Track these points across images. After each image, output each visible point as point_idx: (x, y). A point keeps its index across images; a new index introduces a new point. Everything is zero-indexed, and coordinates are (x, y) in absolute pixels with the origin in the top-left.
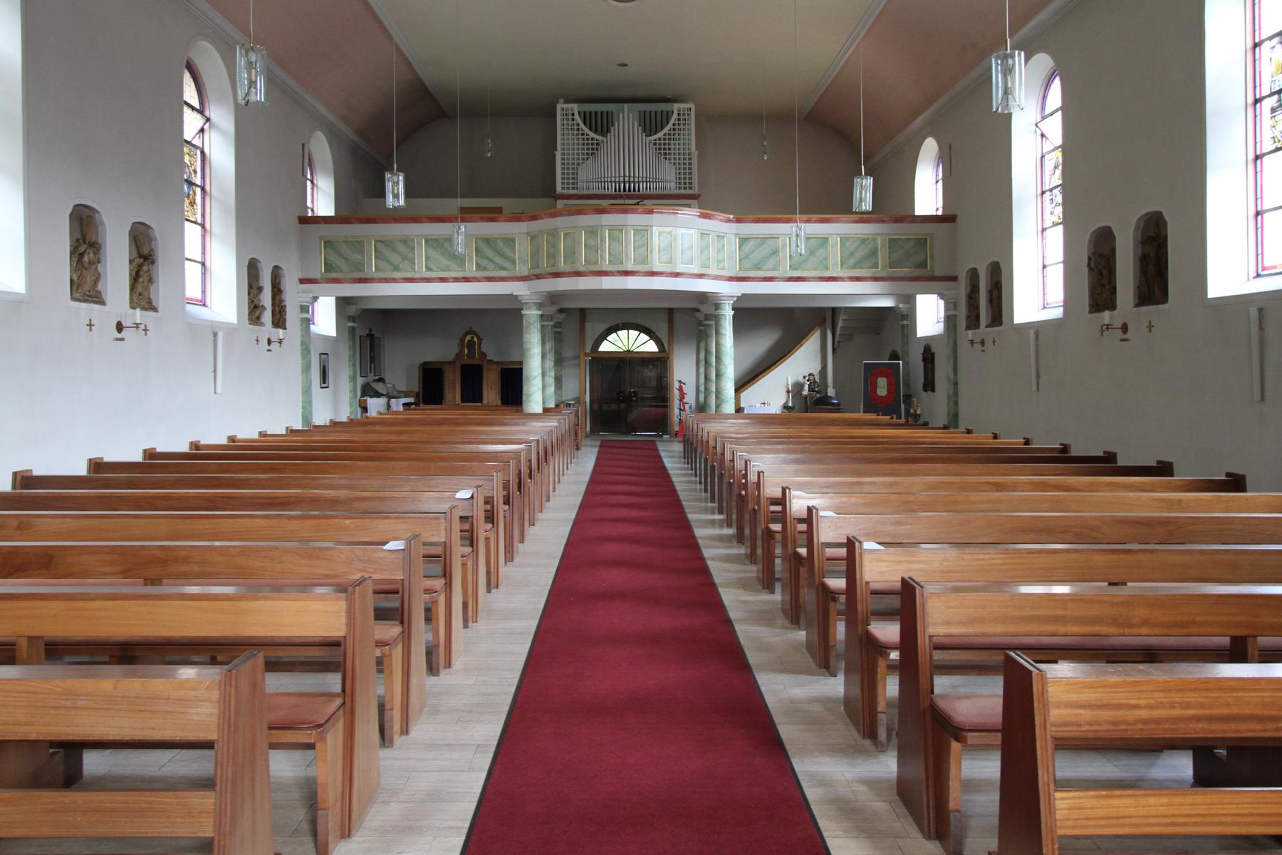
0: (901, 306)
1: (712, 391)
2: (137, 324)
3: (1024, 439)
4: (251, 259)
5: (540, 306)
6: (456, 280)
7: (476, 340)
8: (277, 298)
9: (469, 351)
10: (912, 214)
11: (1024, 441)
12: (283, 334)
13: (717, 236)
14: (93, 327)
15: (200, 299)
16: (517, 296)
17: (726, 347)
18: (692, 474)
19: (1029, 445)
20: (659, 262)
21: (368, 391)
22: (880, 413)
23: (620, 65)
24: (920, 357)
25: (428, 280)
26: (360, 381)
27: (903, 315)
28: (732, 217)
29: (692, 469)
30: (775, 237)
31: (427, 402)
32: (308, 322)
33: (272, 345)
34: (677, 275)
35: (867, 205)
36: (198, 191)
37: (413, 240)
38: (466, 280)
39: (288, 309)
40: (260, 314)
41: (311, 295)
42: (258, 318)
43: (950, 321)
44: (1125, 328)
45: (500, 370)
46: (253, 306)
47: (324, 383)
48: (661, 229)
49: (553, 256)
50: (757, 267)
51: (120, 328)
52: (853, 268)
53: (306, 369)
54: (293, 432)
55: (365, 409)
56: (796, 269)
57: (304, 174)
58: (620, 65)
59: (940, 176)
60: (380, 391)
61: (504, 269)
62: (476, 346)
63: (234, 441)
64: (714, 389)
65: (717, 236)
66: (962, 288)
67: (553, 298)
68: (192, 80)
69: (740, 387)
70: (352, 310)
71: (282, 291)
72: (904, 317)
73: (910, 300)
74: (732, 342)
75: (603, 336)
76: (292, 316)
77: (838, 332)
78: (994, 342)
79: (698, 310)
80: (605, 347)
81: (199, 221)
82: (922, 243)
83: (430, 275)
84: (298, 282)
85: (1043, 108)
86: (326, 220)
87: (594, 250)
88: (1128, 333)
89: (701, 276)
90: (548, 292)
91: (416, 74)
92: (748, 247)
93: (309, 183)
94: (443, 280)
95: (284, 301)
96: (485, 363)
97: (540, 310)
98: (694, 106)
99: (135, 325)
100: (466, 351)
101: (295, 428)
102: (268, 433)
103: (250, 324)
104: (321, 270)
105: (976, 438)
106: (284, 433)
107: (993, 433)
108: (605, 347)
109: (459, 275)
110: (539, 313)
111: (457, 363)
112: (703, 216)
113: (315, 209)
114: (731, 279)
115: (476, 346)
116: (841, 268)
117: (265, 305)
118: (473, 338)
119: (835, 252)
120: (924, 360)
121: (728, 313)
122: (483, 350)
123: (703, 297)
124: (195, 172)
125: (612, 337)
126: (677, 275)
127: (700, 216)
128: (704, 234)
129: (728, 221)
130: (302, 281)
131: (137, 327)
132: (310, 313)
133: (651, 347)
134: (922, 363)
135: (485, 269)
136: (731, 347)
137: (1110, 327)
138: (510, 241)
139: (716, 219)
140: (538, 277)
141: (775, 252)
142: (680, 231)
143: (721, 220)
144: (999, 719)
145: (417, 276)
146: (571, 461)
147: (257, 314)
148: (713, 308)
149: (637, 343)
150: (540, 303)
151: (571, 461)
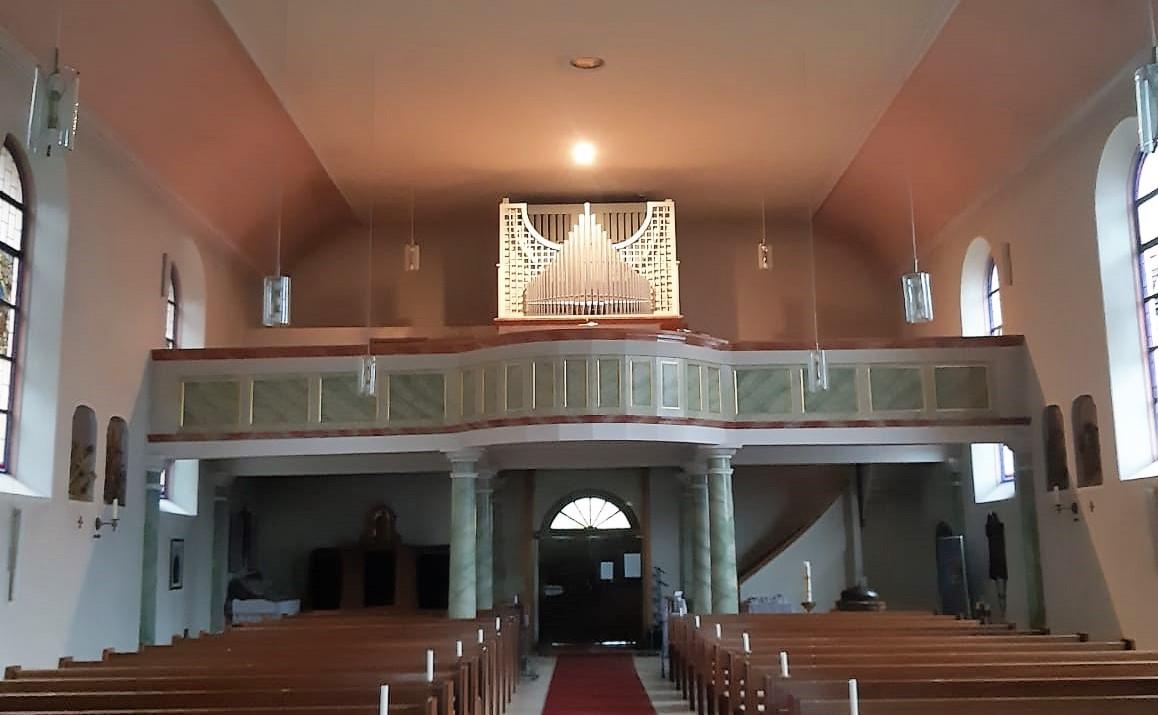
0: (951, 460)
1: (705, 583)
3: (1078, 634)
4: (78, 407)
5: (476, 467)
6: (363, 433)
7: (388, 516)
8: (631, 651)
10: (957, 335)
11: (1123, 643)
12: (119, 511)
13: (709, 368)
16: (443, 453)
17: (724, 519)
18: (686, 706)
19: (1130, 649)
20: (634, 403)
21: (237, 591)
22: (962, 615)
24: (983, 530)
25: (324, 434)
26: (226, 578)
27: (955, 474)
28: (727, 342)
29: (685, 698)
30: (783, 369)
31: (317, 606)
32: (154, 496)
33: (102, 527)
34: (657, 420)
35: (548, 593)
36: (12, 313)
37: (306, 380)
38: (377, 433)
39: (129, 477)
40: (87, 484)
41: (163, 457)
42: (84, 490)
43: (1022, 479)
46: (77, 473)
47: (176, 581)
48: (637, 359)
49: (492, 397)
50: (762, 409)
52: (890, 408)
53: (149, 563)
54: (111, 656)
55: (229, 615)
56: (814, 410)
57: (163, 293)
59: (995, 285)
60: (255, 592)
61: (425, 416)
63: (67, 666)
64: (709, 581)
65: (709, 368)
66: (1037, 433)
67: (492, 453)
68: (14, 165)
69: (745, 570)
70: (221, 479)
71: (121, 453)
72: (956, 476)
73: (963, 454)
74: (732, 512)
75: (557, 509)
76: (134, 486)
77: (867, 496)
78: (1092, 507)
79: (680, 470)
80: (560, 523)
81: (9, 355)
82: (977, 373)
83: (327, 426)
84: (147, 439)
85: (1135, 191)
86: (192, 354)
87: (546, 388)
89: (689, 421)
90: (487, 447)
91: (319, 164)
92: (748, 381)
93: (171, 308)
94: (344, 433)
95: (123, 466)
98: (673, 203)
101: (117, 651)
102: (75, 660)
103: (70, 498)
104: (179, 423)
105: (1054, 640)
106: (100, 659)
107: (1123, 640)
108: (560, 523)
109: (363, 426)
110: (475, 475)
112: (689, 341)
113: (178, 342)
114: (727, 425)
116: (874, 409)
119: (865, 392)
120: (989, 534)
121: (726, 472)
123: (689, 449)
124: (9, 287)
125: (569, 509)
126: (657, 420)
127: (686, 342)
128: (692, 365)
129: (722, 347)
130: (152, 438)
132: (162, 482)
133: (621, 522)
134: (987, 539)
135: (402, 417)
136: (730, 519)
138: (436, 380)
139: (707, 345)
140: (473, 426)
141: (786, 389)
142: (661, 362)
143: (714, 348)
144: (179, 348)
145: (310, 428)
146: (514, 688)
147: (82, 484)
148: (705, 467)
149: (601, 519)
150: (475, 463)
151: (514, 688)
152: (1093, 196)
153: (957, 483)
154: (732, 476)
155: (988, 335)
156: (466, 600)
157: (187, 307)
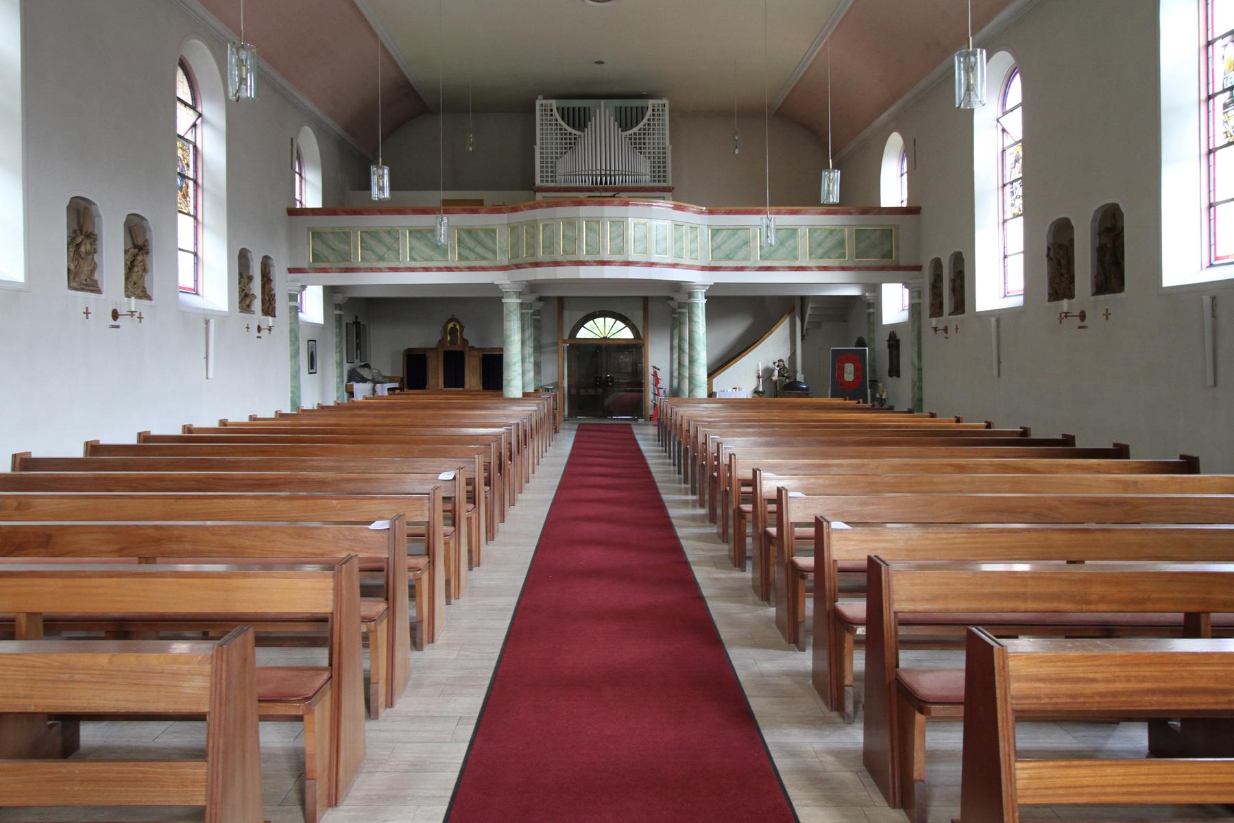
0: (867, 294)
1: (685, 377)
2: (132, 312)
3: (986, 422)
4: (242, 249)
5: (520, 294)
6: (439, 269)
7: (458, 327)
9: (451, 338)
10: (877, 206)
11: (986, 424)
12: (273, 321)
13: (691, 227)
14: (89, 315)
15: (193, 288)
16: (497, 285)
17: (699, 334)
18: (666, 456)
19: (990, 428)
20: (634, 252)
21: (354, 376)
22: (847, 398)
23: (597, 63)
24: (886, 344)
25: (412, 270)
26: (347, 367)
27: (869, 304)
28: (704, 208)
29: (666, 452)
30: (746, 228)
31: (411, 387)
32: (296, 310)
33: (262, 332)
34: (652, 264)
36: (191, 183)
37: (397, 231)
38: (449, 269)
39: (277, 298)
40: (250, 302)
41: (299, 284)
42: (249, 306)
43: (914, 309)
44: (1082, 316)
45: (481, 356)
46: (243, 295)
47: (312, 368)
48: (636, 220)
49: (532, 247)
50: (728, 257)
51: (115, 315)
52: (821, 258)
53: (295, 355)
54: (282, 416)
55: (351, 394)
56: (766, 259)
57: (293, 168)
58: (597, 63)
59: (905, 169)
60: (366, 376)
61: (485, 259)
62: (459, 333)
63: (225, 425)
64: (687, 375)
65: (691, 227)
66: (926, 278)
67: (533, 286)
68: (184, 77)
70: (339, 298)
71: (271, 281)
72: (870, 305)
73: (876, 289)
74: (705, 329)
75: (581, 324)
76: (281, 304)
77: (807, 320)
78: (957, 329)
79: (672, 299)
80: (583, 334)
81: (192, 213)
82: (887, 234)
83: (414, 264)
84: (287, 271)
85: (1004, 104)
86: (313, 212)
87: (572, 240)
88: (1086, 321)
89: (675, 266)
90: (527, 281)
91: (401, 72)
92: (720, 237)
93: (297, 176)
94: (426, 269)
95: (273, 290)
96: (467, 350)
97: (520, 298)
98: (668, 102)
99: (130, 313)
100: (449, 338)
101: (284, 412)
102: (258, 417)
103: (240, 312)
104: (309, 260)
106: (273, 417)
107: (956, 417)
108: (583, 334)
109: (442, 264)
110: (519, 301)
111: (440, 349)
112: (677, 208)
113: (303, 202)
114: (704, 268)
115: (459, 333)
116: (810, 258)
117: (255, 294)
118: (455, 325)
119: (803, 243)
120: (890, 346)
121: (700, 301)
122: (465, 337)
123: (677, 286)
124: (188, 165)
125: (589, 324)
126: (652, 264)
127: (673, 208)
128: (678, 226)
129: (701, 212)
130: (291, 271)
131: (132, 315)
132: (299, 301)
133: (627, 334)
134: (888, 350)
135: (467, 259)
136: (703, 334)
137: (1068, 314)
138: (491, 232)
139: (689, 211)
140: (518, 266)
141: (746, 243)
142: (655, 223)
143: (694, 212)
145: (401, 266)
146: (549, 443)
147: (247, 302)
148: (687, 296)
149: (614, 331)
150: (520, 292)
151: (549, 443)
152: (882, 160)
153: (871, 310)
154: (706, 304)
155: (899, 206)
156: (517, 379)
157: (206, 108)
